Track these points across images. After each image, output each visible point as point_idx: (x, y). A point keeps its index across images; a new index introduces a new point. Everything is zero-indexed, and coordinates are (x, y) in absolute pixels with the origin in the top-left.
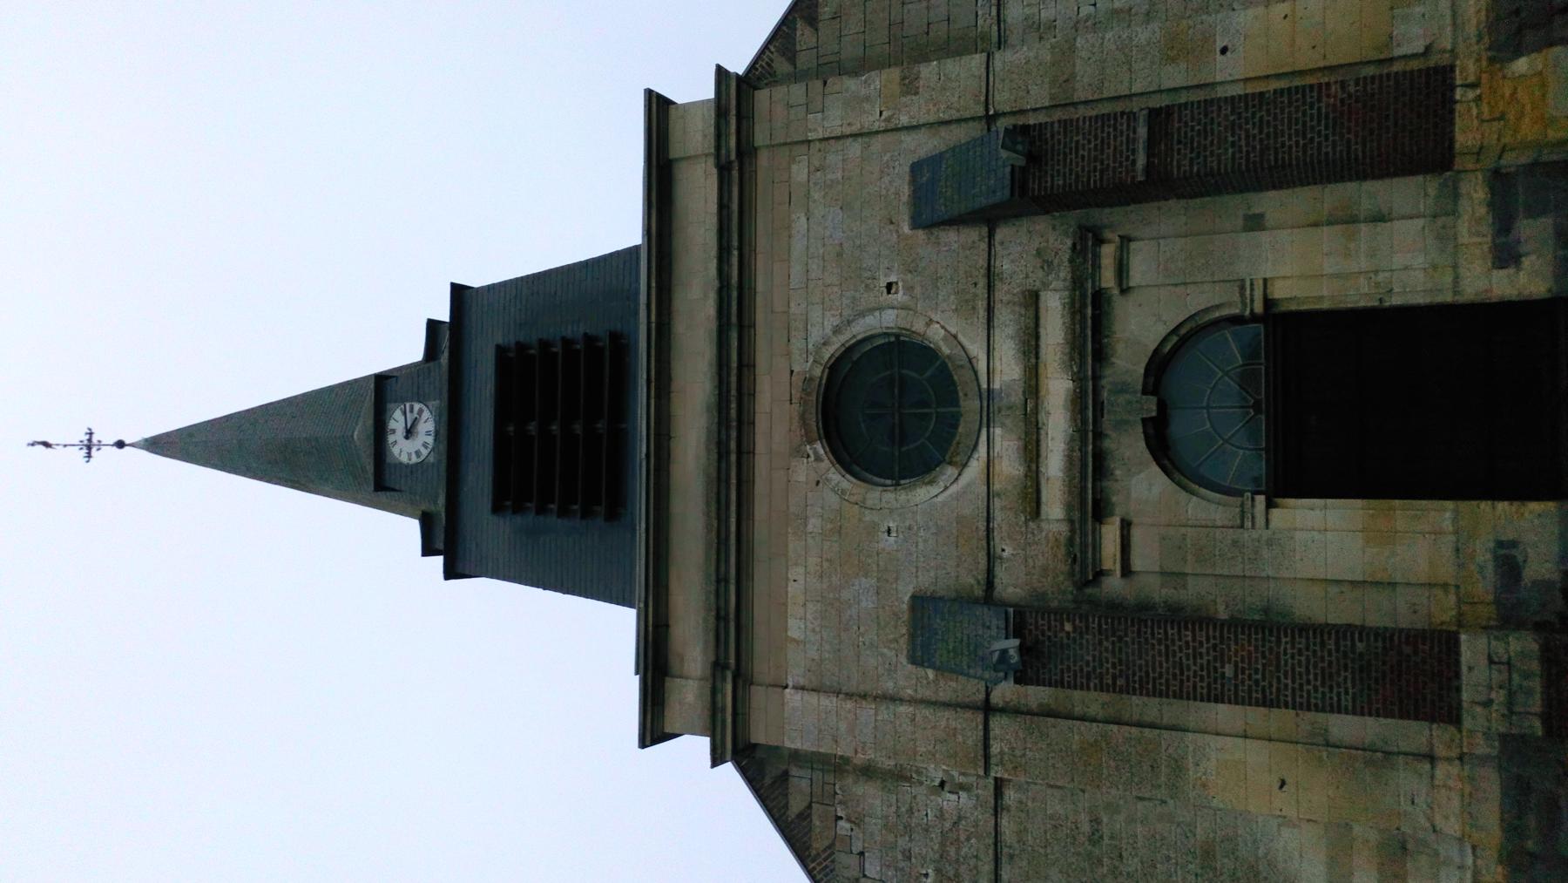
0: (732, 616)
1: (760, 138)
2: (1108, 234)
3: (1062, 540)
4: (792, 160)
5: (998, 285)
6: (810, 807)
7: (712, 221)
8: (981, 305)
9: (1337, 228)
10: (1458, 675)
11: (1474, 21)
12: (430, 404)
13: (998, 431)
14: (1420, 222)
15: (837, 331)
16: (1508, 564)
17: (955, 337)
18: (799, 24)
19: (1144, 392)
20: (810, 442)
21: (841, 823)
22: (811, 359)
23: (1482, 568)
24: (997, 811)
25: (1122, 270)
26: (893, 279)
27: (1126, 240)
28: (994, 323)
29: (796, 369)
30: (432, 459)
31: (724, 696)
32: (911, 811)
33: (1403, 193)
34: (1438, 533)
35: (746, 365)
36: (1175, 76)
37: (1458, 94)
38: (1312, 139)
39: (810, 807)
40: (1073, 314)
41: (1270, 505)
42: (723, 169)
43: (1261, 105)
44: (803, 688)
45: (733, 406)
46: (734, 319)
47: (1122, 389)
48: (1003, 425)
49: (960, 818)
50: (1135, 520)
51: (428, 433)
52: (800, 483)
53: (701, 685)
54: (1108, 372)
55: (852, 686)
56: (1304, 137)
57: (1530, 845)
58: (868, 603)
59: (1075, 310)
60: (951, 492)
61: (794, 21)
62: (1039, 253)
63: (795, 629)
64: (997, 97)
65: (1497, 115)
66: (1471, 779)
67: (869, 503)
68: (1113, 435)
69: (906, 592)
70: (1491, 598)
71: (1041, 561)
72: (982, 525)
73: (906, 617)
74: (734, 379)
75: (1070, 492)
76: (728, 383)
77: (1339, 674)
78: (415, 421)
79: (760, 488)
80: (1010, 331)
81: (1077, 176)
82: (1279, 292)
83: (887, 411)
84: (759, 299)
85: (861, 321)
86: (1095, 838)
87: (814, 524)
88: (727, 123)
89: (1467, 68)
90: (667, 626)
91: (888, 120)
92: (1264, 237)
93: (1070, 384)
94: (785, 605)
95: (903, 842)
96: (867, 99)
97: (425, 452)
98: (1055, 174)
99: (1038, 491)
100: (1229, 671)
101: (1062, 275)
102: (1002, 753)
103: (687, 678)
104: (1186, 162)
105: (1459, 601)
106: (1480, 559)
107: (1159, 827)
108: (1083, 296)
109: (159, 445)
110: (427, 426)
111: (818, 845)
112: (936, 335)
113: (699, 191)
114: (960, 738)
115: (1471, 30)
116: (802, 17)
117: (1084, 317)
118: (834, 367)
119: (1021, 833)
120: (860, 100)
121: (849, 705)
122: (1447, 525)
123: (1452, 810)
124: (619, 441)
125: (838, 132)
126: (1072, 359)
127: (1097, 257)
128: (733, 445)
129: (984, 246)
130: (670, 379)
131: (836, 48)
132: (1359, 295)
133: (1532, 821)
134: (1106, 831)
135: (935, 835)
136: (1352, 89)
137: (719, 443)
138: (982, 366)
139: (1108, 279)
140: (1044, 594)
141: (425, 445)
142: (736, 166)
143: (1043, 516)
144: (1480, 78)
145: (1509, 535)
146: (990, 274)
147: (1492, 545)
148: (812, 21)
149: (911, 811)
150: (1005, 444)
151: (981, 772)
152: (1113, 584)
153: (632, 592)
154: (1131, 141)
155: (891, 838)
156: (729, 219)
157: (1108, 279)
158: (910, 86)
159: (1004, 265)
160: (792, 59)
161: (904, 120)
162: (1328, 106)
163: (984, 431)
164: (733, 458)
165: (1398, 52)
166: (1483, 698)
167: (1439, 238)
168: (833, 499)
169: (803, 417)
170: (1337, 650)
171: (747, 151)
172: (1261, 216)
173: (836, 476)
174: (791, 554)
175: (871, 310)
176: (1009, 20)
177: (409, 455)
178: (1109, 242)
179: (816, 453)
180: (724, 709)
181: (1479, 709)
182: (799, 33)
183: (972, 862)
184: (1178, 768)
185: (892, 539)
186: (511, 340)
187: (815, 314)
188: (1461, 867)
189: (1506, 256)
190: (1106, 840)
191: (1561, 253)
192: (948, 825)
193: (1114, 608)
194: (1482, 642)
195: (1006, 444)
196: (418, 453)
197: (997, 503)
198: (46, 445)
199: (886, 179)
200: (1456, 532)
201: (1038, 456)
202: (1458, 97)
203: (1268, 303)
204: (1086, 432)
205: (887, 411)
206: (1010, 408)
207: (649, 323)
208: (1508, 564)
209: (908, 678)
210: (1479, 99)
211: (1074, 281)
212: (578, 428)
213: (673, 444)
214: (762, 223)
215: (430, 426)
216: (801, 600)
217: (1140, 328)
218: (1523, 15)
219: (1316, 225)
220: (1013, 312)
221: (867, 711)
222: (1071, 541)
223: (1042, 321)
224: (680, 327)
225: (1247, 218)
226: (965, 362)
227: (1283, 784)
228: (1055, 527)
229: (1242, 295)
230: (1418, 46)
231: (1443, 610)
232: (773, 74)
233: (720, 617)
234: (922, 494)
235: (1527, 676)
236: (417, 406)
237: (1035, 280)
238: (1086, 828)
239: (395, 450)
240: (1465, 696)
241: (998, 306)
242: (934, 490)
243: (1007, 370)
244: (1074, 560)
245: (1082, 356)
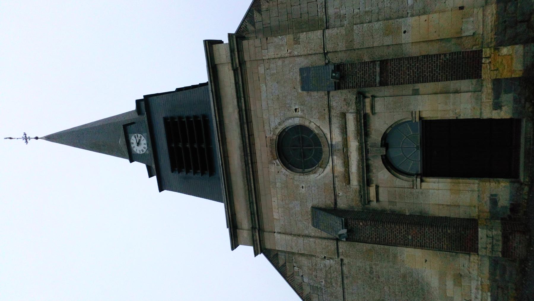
0: (256, 213)
1: (246, 58)
2: (367, 95)
3: (358, 191)
4: (258, 66)
5: (332, 111)
6: (285, 263)
7: (233, 86)
8: (327, 117)
9: (444, 95)
10: (477, 240)
11: (490, 24)
12: (144, 134)
13: (335, 157)
14: (470, 94)
15: (280, 124)
16: (494, 201)
17: (319, 127)
18: (255, 12)
19: (381, 146)
20: (275, 160)
21: (295, 268)
22: (272, 133)
23: (486, 202)
24: (342, 265)
25: (372, 107)
26: (297, 107)
27: (373, 97)
28: (331, 122)
29: (268, 136)
30: (148, 152)
31: (256, 237)
32: (316, 265)
33: (465, 84)
34: (473, 191)
35: (251, 135)
36: (388, 41)
37: (483, 61)
38: (435, 74)
39: (285, 263)
40: (357, 121)
41: (422, 181)
42: (235, 70)
43: (418, 60)
44: (280, 233)
45: (248, 149)
46: (245, 121)
47: (374, 145)
48: (336, 155)
49: (331, 267)
50: (380, 185)
51: (145, 144)
52: (274, 174)
53: (248, 228)
54: (369, 140)
55: (296, 232)
56: (432, 73)
57: (497, 278)
58: (298, 209)
59: (358, 121)
60: (320, 176)
61: (253, 11)
62: (345, 100)
63: (276, 216)
64: (327, 47)
65: (496, 69)
66: (481, 260)
67: (296, 179)
68: (372, 159)
69: (310, 205)
70: (488, 210)
71: (351, 197)
72: (332, 186)
73: (310, 213)
74: (247, 141)
75: (359, 177)
76: (246, 142)
77: (442, 239)
78: (140, 140)
79: (260, 173)
80: (337, 125)
81: (357, 84)
82: (425, 115)
83: (299, 149)
84: (253, 113)
85: (288, 121)
86: (371, 272)
87: (278, 185)
88: (235, 54)
89: (487, 52)
90: (235, 214)
91: (290, 53)
92: (419, 97)
93: (358, 144)
94: (272, 208)
95: (314, 273)
96: (282, 45)
97: (145, 150)
98: (350, 76)
99: (349, 177)
100: (410, 237)
101: (353, 107)
102: (342, 252)
103: (243, 229)
104: (393, 80)
105: (479, 211)
106: (485, 199)
107: (390, 269)
108: (360, 116)
109: (49, 138)
110: (144, 141)
111: (289, 274)
112: (312, 126)
113: (227, 76)
114: (329, 248)
115: (489, 28)
116: (255, 10)
117: (361, 124)
118: (280, 135)
119: (349, 271)
120: (279, 46)
121: (295, 238)
122: (476, 189)
123: (475, 268)
124: (210, 152)
125: (273, 57)
126: (358, 136)
127: (364, 102)
128: (250, 161)
129: (326, 97)
130: (226, 139)
131: (269, 22)
132: (451, 116)
133: (498, 272)
134: (374, 270)
135: (324, 271)
136: (448, 57)
137: (245, 161)
138: (328, 136)
139: (368, 110)
140: (353, 207)
141: (144, 148)
142: (239, 69)
143: (351, 184)
144: (491, 55)
145: (494, 193)
146: (329, 107)
147: (489, 195)
148: (259, 11)
149: (316, 265)
150: (338, 162)
151: (337, 257)
152: (374, 204)
153: (222, 198)
154: (374, 72)
155: (311, 272)
156: (239, 87)
157: (368, 110)
158: (297, 41)
159: (334, 104)
160: (254, 25)
161: (296, 53)
162: (440, 62)
163: (331, 157)
164: (250, 165)
165: (463, 35)
166: (484, 246)
167: (477, 99)
168: (284, 177)
169: (271, 151)
170: (442, 232)
171: (242, 63)
172: (418, 90)
173: (284, 170)
174: (272, 194)
175: (290, 118)
176: (329, 14)
177: (140, 151)
178: (368, 97)
179: (277, 163)
180: (256, 240)
181: (483, 250)
182: (255, 15)
183: (335, 278)
184: (395, 256)
185: (304, 190)
186: (169, 115)
187: (272, 118)
188: (477, 280)
189: (497, 106)
190: (374, 273)
191: (515, 106)
192: (327, 269)
193: (375, 212)
194: (485, 231)
195: (338, 161)
196: (142, 151)
197: (336, 179)
198: (11, 138)
199: (292, 73)
200: (479, 191)
201: (348, 166)
202: (483, 62)
203: (420, 118)
204: (363, 159)
205: (299, 149)
206: (338, 150)
207: (216, 121)
208: (494, 201)
209: (312, 230)
210: (490, 62)
211: (357, 110)
212: (196, 146)
213: (230, 159)
214: (250, 87)
215: (145, 142)
216: (277, 207)
217: (379, 125)
218: (507, 23)
219: (436, 93)
220: (337, 119)
221: (301, 240)
222: (360, 191)
223: (347, 123)
224: (226, 121)
225: (413, 90)
226: (322, 135)
227: (426, 261)
228: (355, 187)
229: (412, 116)
230: (471, 33)
231: (474, 213)
232: (247, 31)
233: (252, 214)
234: (312, 177)
235: (497, 241)
236: (139, 135)
237: (344, 109)
238: (369, 270)
239: (135, 149)
240: (479, 246)
241: (332, 117)
242: (316, 175)
243: (337, 138)
244: (362, 197)
245: (361, 136)
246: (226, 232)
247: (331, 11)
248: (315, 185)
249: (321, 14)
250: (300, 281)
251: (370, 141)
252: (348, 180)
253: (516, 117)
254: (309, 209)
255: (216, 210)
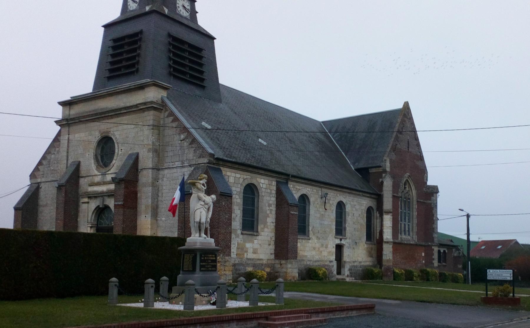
53: (75, 113)
55: (70, 150)
97: (179, 9)
103: (69, 111)
112: (114, 162)
138: (109, 172)
141: (179, 7)
187: (119, 133)
246: (67, 98)
247: (166, 171)
248: (89, 165)
249: (166, 165)
250: (53, 153)
251: (106, 198)
252: (92, 184)
253: (298, 258)
254: (79, 160)
255: (87, 87)
